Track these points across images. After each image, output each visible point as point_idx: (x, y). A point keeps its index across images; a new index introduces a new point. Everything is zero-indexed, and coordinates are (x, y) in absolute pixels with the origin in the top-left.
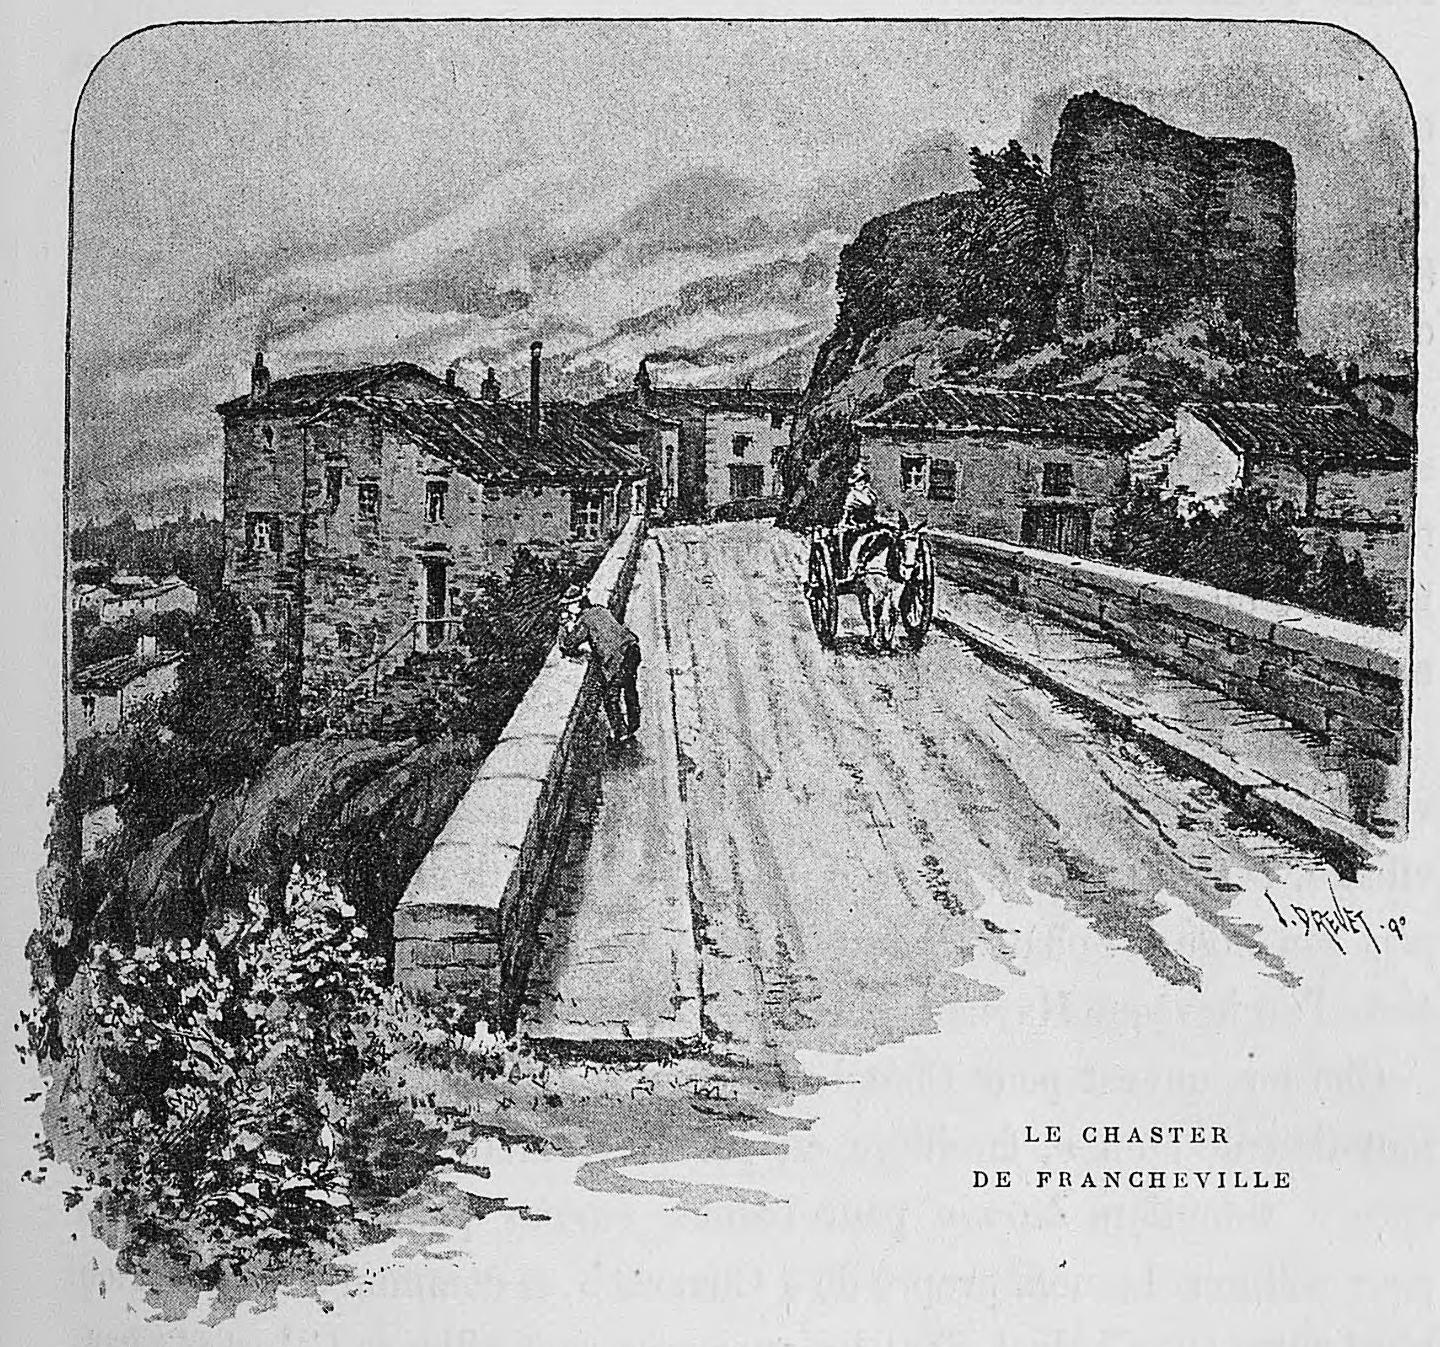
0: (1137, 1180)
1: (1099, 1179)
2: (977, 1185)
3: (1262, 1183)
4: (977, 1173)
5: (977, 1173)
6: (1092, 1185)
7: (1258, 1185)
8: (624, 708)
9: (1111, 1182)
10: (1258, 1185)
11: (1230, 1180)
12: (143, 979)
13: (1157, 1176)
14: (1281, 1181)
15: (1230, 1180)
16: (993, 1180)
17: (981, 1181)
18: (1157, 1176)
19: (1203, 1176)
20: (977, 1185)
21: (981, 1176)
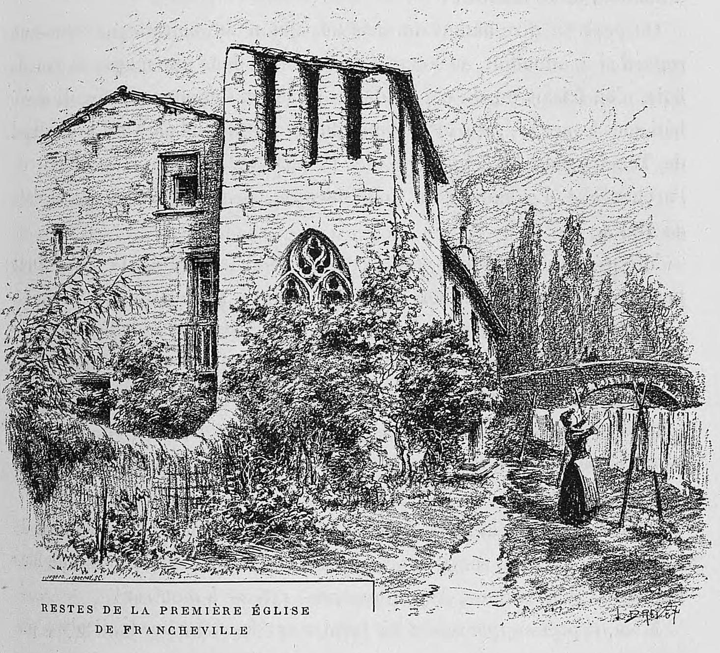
0: (172, 631)
1: (155, 630)
2: (105, 613)
3: (278, 612)
4: (105, 607)
5: (105, 607)
6: (203, 628)
7: (276, 614)
8: (202, 347)
9: (160, 631)
10: (276, 614)
11: (218, 630)
12: (450, 417)
13: (183, 629)
14: (305, 611)
15: (218, 630)
16: (113, 610)
17: (267, 610)
18: (183, 629)
19: (205, 629)
20: (105, 613)
21: (107, 608)
